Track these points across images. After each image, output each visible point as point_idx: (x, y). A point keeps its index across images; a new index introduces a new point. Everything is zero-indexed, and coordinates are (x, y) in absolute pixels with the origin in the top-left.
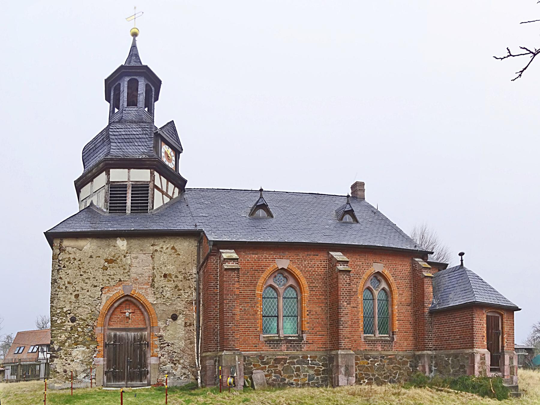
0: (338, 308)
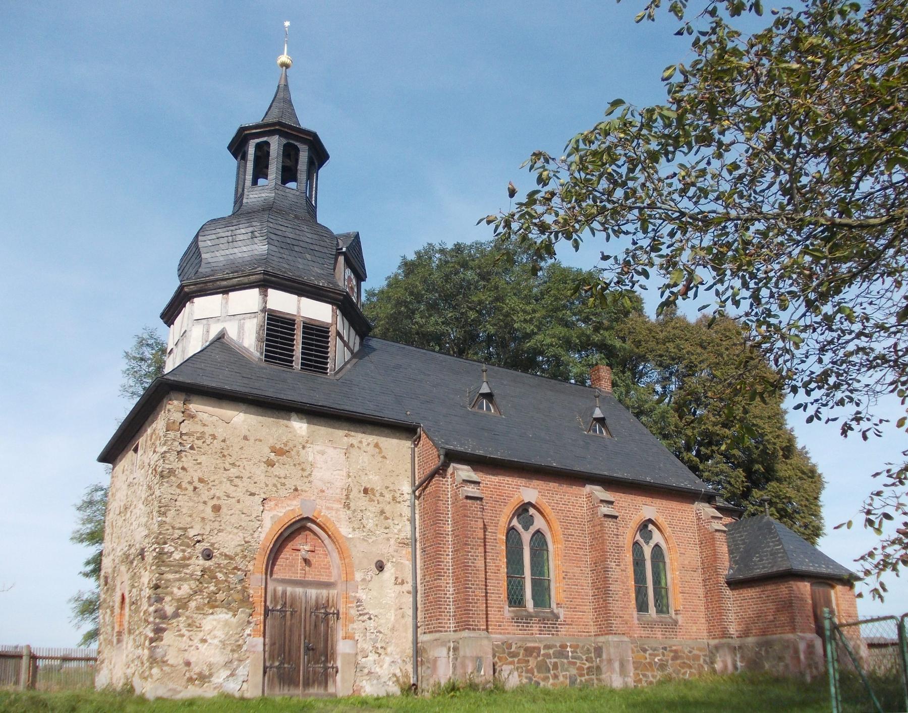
0: (606, 570)
